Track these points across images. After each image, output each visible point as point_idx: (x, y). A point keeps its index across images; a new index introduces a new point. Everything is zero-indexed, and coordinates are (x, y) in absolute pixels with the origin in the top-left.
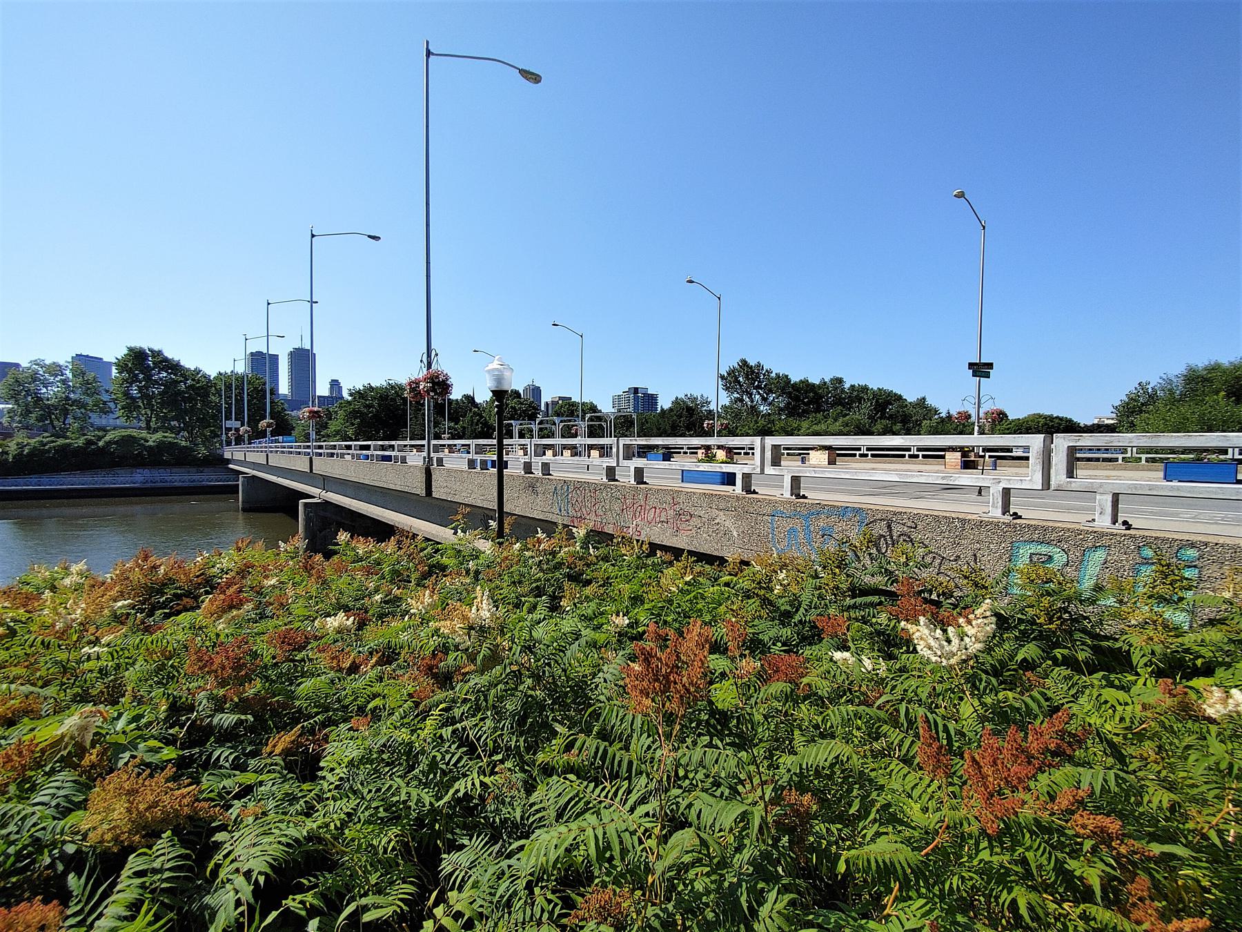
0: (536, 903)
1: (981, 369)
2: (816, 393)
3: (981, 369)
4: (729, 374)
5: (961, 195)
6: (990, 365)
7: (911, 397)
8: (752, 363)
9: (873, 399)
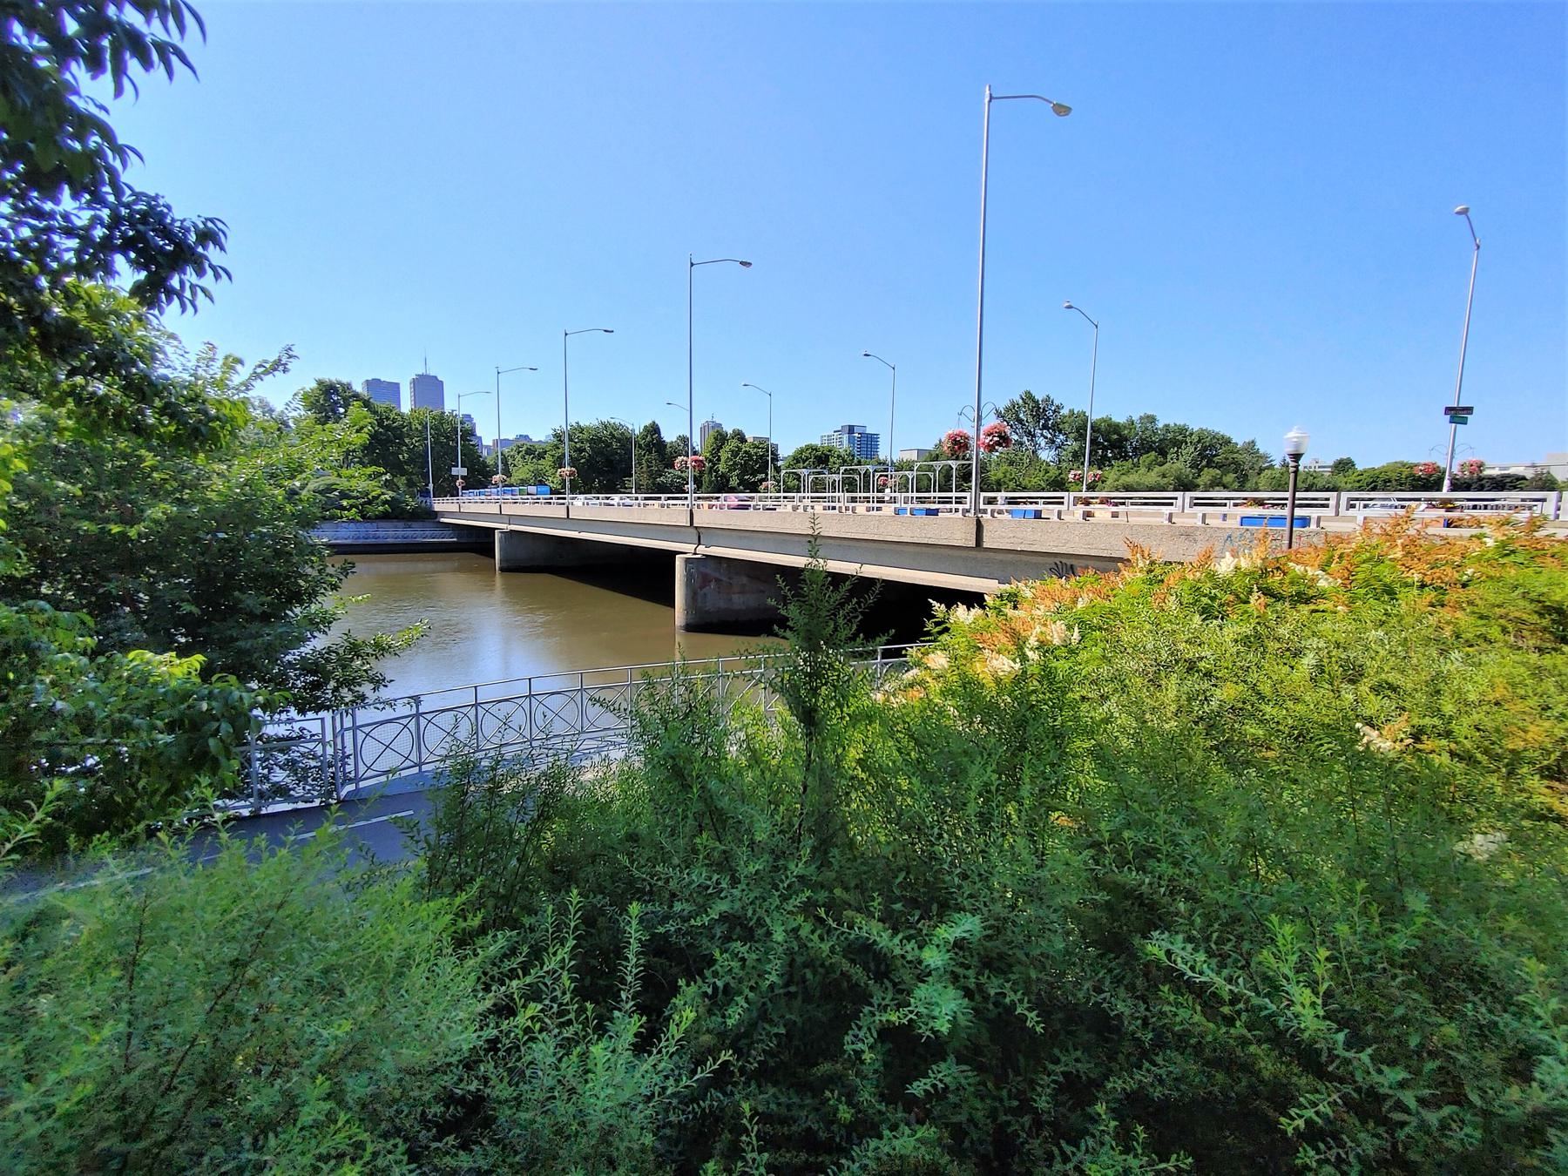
0: (1556, 784)
1: (1458, 414)
2: (1119, 434)
3: (1458, 414)
4: (1008, 409)
5: (1465, 212)
6: (1469, 410)
7: (1239, 439)
8: (1039, 397)
9: (1199, 442)
